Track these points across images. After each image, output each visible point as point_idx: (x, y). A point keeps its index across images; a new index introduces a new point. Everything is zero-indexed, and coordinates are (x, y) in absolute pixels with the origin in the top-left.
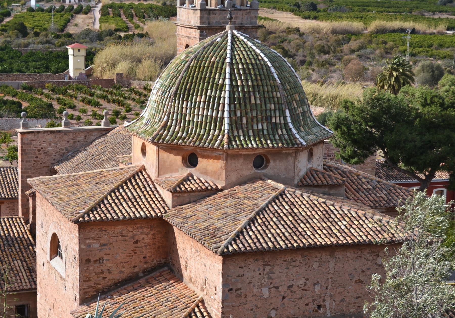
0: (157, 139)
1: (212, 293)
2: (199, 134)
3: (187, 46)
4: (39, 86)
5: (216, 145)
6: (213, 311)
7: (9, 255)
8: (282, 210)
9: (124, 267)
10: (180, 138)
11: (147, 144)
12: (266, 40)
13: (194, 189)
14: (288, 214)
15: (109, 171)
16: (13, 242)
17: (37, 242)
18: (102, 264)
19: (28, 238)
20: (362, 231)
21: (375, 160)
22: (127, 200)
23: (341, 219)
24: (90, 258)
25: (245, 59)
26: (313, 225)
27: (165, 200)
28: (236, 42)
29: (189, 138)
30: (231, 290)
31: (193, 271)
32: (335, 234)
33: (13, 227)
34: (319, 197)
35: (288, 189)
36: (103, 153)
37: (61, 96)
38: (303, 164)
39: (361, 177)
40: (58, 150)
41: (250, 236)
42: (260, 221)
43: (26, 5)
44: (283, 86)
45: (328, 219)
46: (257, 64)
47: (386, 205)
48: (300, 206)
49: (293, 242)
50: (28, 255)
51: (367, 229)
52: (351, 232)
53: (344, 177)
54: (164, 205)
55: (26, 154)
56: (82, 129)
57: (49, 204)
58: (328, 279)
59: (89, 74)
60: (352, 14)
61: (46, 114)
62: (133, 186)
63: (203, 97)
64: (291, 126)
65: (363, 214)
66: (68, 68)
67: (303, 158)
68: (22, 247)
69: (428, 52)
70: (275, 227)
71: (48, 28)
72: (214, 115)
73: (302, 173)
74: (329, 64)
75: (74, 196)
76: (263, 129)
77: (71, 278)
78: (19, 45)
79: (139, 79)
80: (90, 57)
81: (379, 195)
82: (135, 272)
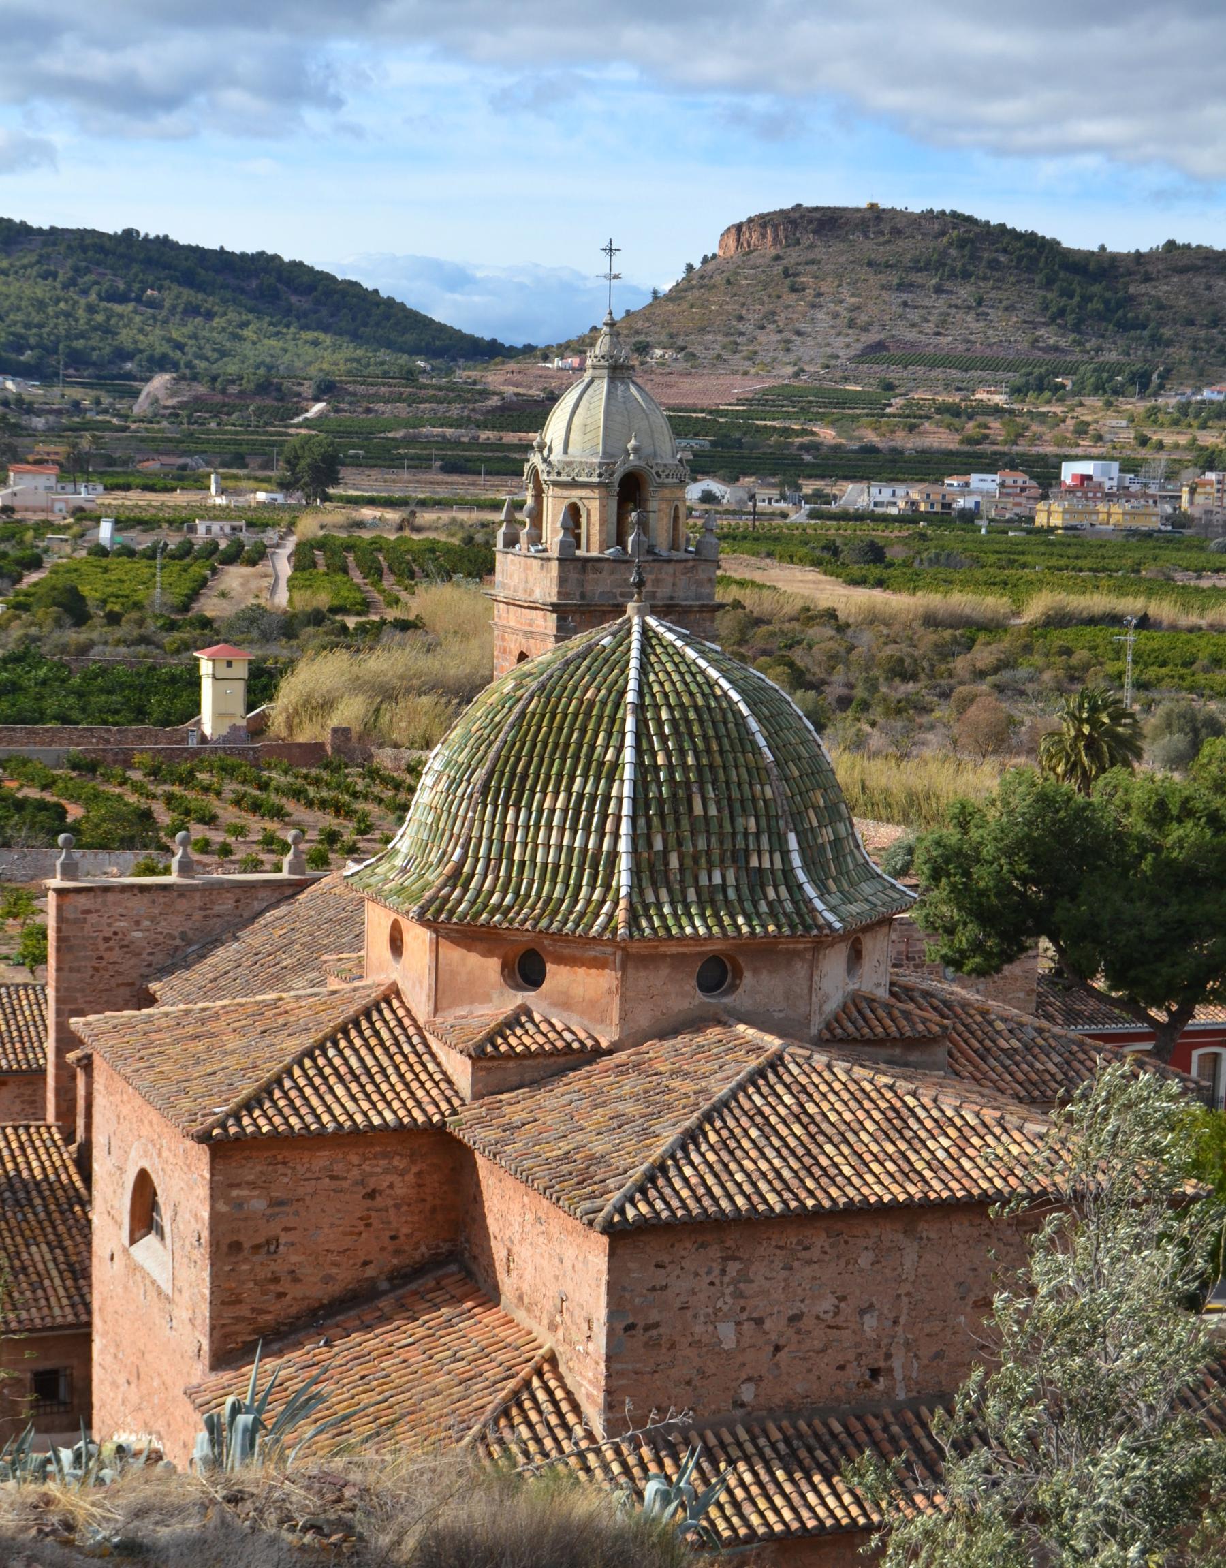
0: (432, 909)
1: (578, 1336)
2: (549, 898)
3: (522, 657)
4: (115, 762)
6: (581, 1385)
7: (15, 1231)
8: (773, 1108)
9: (337, 1265)
10: (498, 907)
11: (405, 923)
12: (746, 642)
13: (533, 1047)
14: (790, 1119)
15: (299, 998)
16: (28, 1192)
17: (94, 1193)
19: (72, 1183)
21: (1034, 970)
22: (348, 1078)
23: (936, 1132)
24: (242, 1239)
25: (678, 693)
26: (859, 1148)
27: (454, 1078)
28: (653, 647)
29: (521, 909)
30: (630, 1327)
31: (527, 1276)
32: (919, 1173)
33: (29, 1151)
34: (878, 1071)
35: (791, 1050)
36: (284, 949)
37: (176, 789)
38: (834, 982)
39: (993, 1017)
40: (161, 939)
41: (686, 1180)
42: (713, 1137)
43: (87, 538)
45: (900, 1132)
46: (709, 708)
48: (824, 1095)
49: (803, 1195)
50: (69, 1230)
52: (961, 1168)
53: (947, 1018)
54: (449, 1093)
55: (70, 949)
56: (229, 881)
57: (130, 1090)
58: (899, 1296)
59: (258, 728)
60: (979, 574)
61: (132, 838)
62: (366, 1040)
63: (562, 795)
64: (802, 877)
66: (199, 713)
67: (834, 963)
68: (53, 1207)
70: (754, 1154)
71: (146, 602)
73: (832, 1006)
76: (724, 887)
77: (186, 1295)
78: (64, 649)
79: (396, 746)
80: (261, 684)
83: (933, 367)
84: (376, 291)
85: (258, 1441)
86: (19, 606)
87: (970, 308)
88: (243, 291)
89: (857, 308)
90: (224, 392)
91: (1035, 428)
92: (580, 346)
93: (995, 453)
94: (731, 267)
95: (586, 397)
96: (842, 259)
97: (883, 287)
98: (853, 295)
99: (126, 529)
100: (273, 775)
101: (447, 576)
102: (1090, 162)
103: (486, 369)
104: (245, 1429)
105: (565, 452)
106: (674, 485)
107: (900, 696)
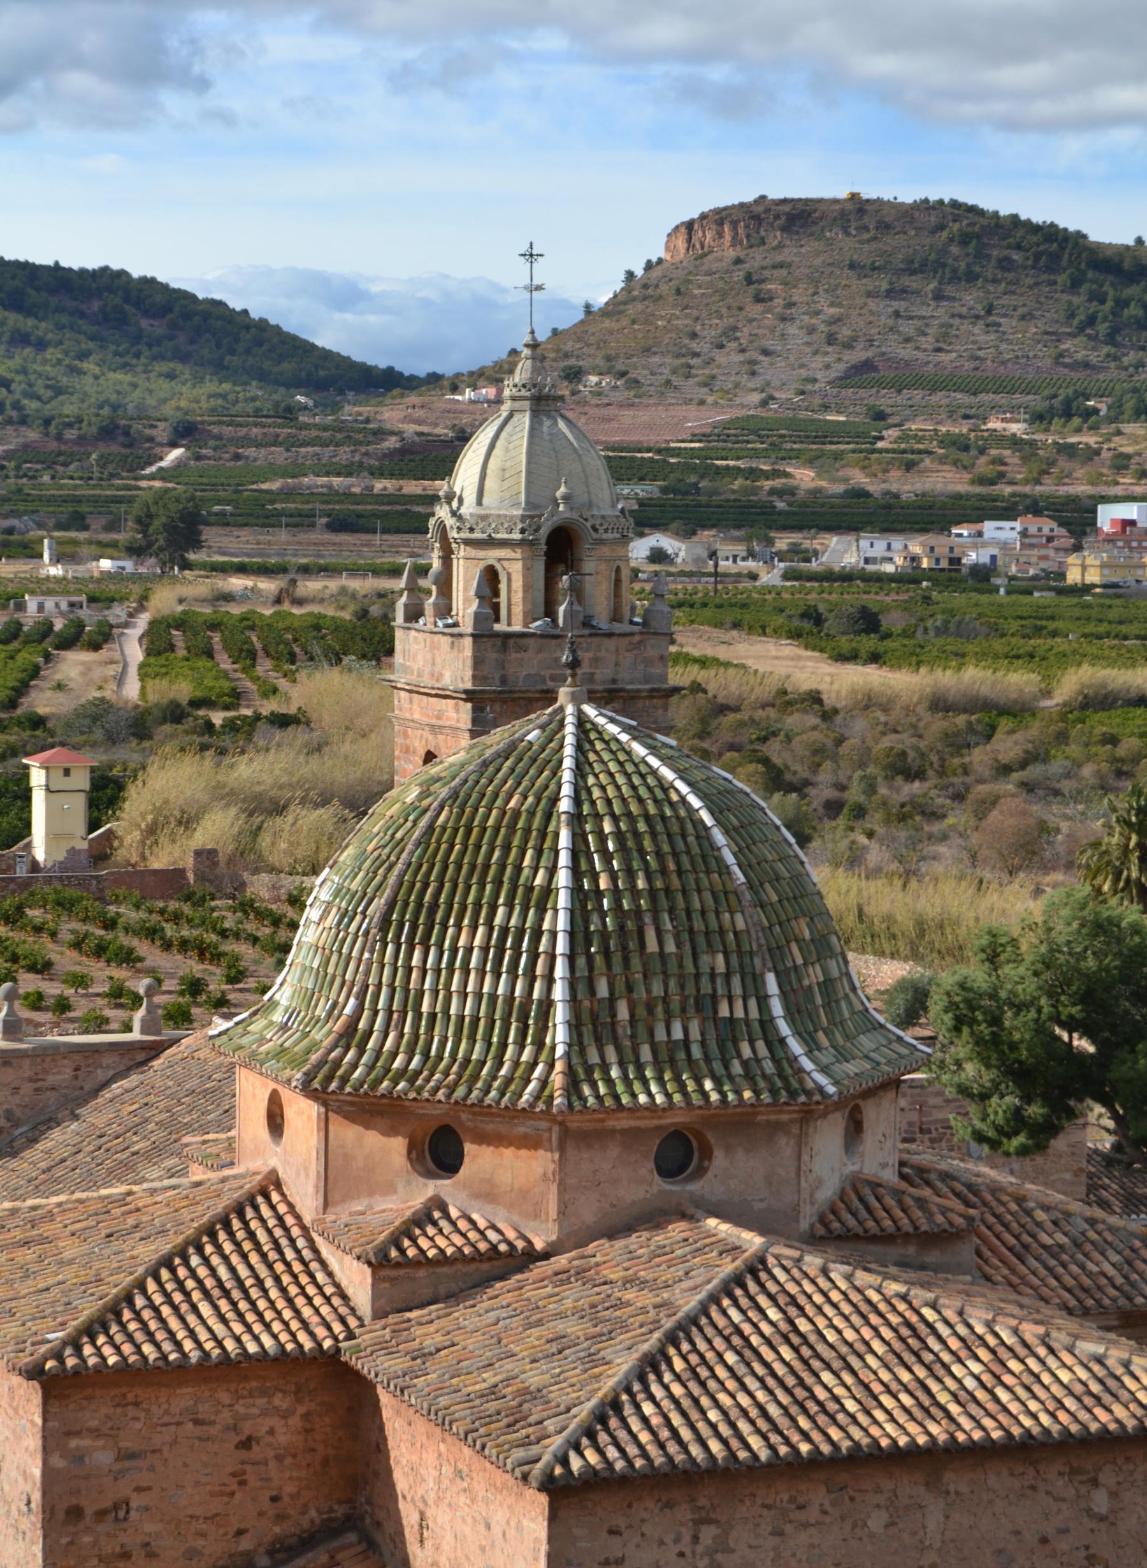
0: (320, 1076)
2: (467, 1060)
3: (429, 757)
5: (525, 1097)
8: (755, 1326)
9: (203, 1535)
11: (286, 1094)
12: (709, 734)
13: (449, 1251)
14: (777, 1340)
15: (153, 1192)
18: (124, 1525)
20: (1035, 1397)
21: (1082, 1143)
22: (216, 1293)
23: (963, 1354)
24: (84, 1503)
25: (624, 800)
27: (350, 1292)
28: (591, 743)
31: (445, 1547)
34: (886, 1277)
35: (776, 1250)
36: (135, 1129)
38: (828, 1163)
39: (1032, 1204)
41: (645, 1420)
42: (679, 1364)
44: (756, 893)
45: (917, 1355)
46: (663, 818)
47: (1122, 1302)
49: (795, 1437)
51: (1056, 1389)
52: (997, 1400)
53: (974, 1207)
54: (343, 1310)
59: (100, 854)
60: (998, 645)
62: (238, 1244)
63: (481, 930)
64: (784, 1029)
65: (1038, 1336)
66: (29, 834)
70: (731, 1385)
72: (517, 993)
73: (827, 1192)
74: (923, 813)
75: (30, 1282)
76: (686, 1043)
79: (273, 870)
80: (105, 795)
81: (1095, 1269)
82: (241, 1554)
84: (245, 312)
87: (977, 317)
88: (83, 315)
89: (837, 320)
90: (59, 437)
92: (495, 374)
93: (1014, 495)
94: (681, 273)
95: (504, 435)
96: (818, 262)
97: (869, 294)
98: (832, 305)
100: (122, 910)
101: (336, 659)
103: (381, 404)
105: (479, 502)
106: (615, 542)
107: (903, 798)
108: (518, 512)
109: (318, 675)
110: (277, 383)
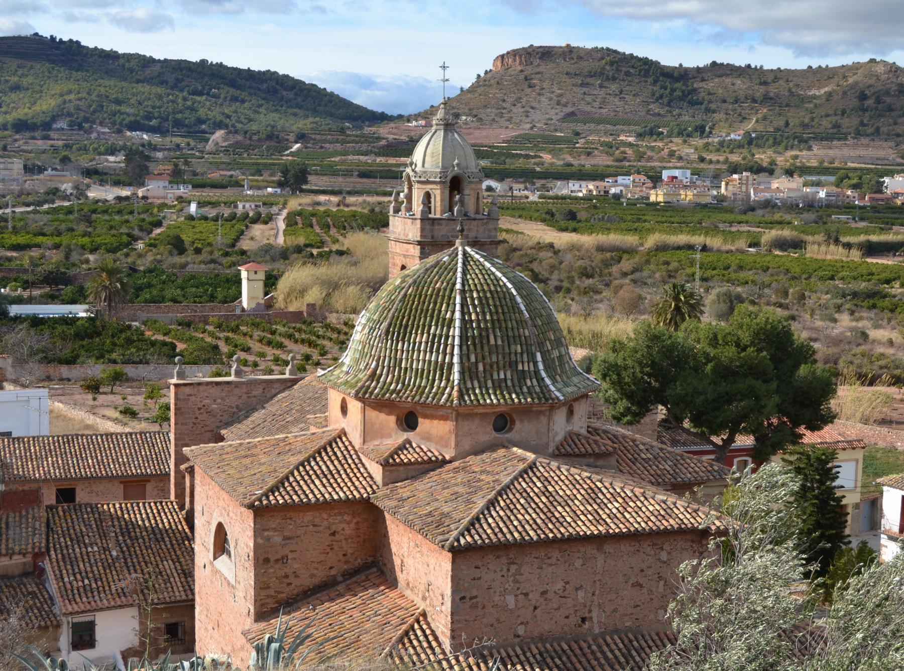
1: (437, 601)
2: (420, 386)
3: (403, 267)
9: (317, 569)
10: (394, 391)
11: (348, 399)
13: (413, 460)
14: (540, 494)
15: (296, 437)
16: (162, 535)
20: (639, 516)
21: (656, 419)
22: (321, 476)
23: (612, 500)
24: (270, 556)
25: (481, 284)
27: (374, 476)
30: (463, 598)
31: (411, 573)
32: (604, 520)
33: (162, 514)
34: (582, 470)
35: (540, 460)
36: (287, 412)
37: (230, 335)
38: (560, 426)
41: (489, 525)
42: (502, 503)
46: (497, 291)
47: (672, 480)
49: (547, 531)
51: (647, 513)
52: (625, 517)
54: (371, 483)
59: (269, 305)
60: (623, 225)
61: (209, 359)
62: (330, 457)
63: (425, 335)
64: (544, 374)
67: (560, 417)
68: (174, 542)
69: (723, 275)
70: (522, 511)
73: (560, 438)
76: (505, 379)
77: (242, 584)
78: (174, 266)
79: (337, 312)
80: (271, 281)
83: (599, 124)
84: (325, 89)
85: (282, 656)
86: (151, 245)
88: (259, 90)
89: (561, 95)
90: (250, 139)
91: (649, 153)
92: (427, 115)
96: (553, 72)
97: (574, 85)
99: (203, 207)
101: (361, 228)
102: (679, 23)
104: (275, 650)
105: (423, 166)
106: (477, 182)
108: (439, 170)
109: (355, 235)
110: (337, 118)
